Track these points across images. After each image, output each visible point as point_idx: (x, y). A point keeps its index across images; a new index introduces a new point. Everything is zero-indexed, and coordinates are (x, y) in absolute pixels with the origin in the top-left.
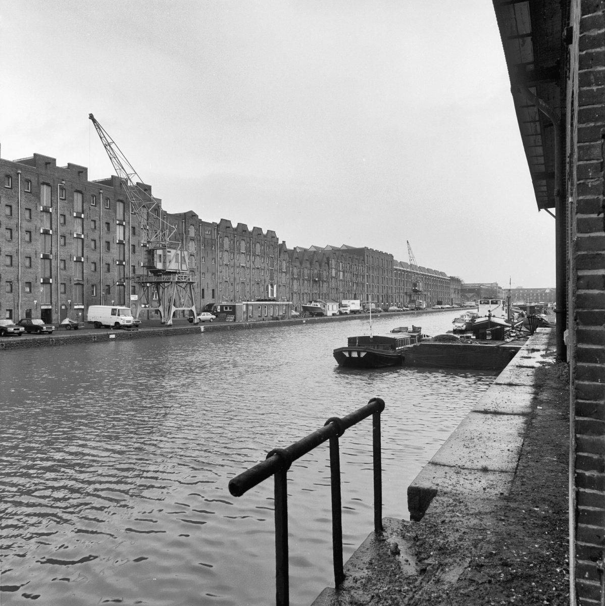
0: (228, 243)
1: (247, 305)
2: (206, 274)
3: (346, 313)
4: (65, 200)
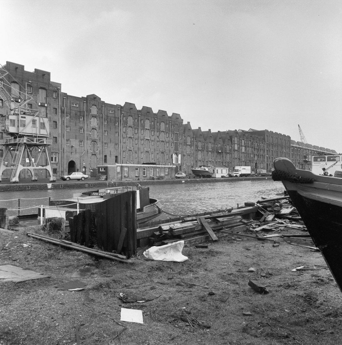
0: (237, 146)
1: (122, 167)
2: (109, 145)
3: (236, 176)
4: (32, 94)
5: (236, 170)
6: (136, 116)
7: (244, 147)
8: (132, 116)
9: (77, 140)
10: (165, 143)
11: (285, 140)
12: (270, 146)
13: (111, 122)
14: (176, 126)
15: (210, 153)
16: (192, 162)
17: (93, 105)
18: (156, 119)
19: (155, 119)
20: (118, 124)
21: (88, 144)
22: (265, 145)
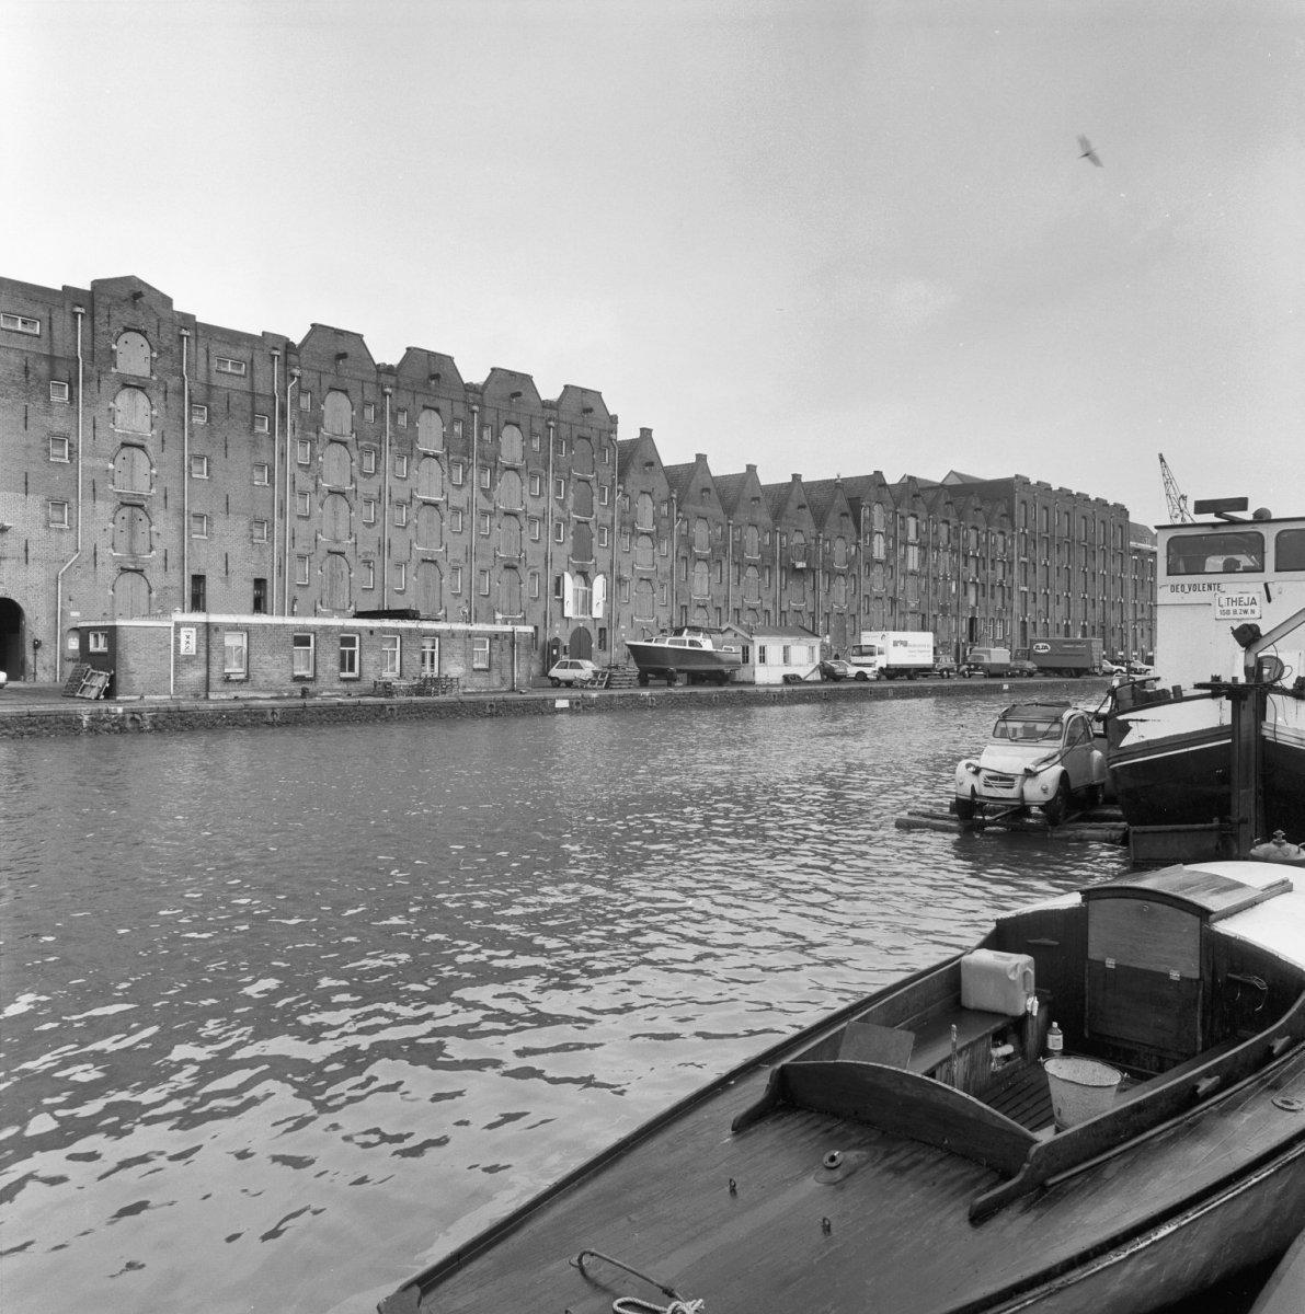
0: (882, 545)
1: (208, 629)
2: (219, 524)
3: (861, 677)
5: (864, 650)
6: (366, 392)
7: (916, 548)
8: (345, 392)
9: (30, 496)
10: (526, 524)
11: (1103, 522)
12: (1035, 547)
13: (228, 414)
14: (579, 444)
15: (751, 572)
16: (664, 609)
17: (127, 330)
18: (476, 408)
19: (473, 412)
20: (272, 429)
21: (97, 522)
22: (1013, 544)
